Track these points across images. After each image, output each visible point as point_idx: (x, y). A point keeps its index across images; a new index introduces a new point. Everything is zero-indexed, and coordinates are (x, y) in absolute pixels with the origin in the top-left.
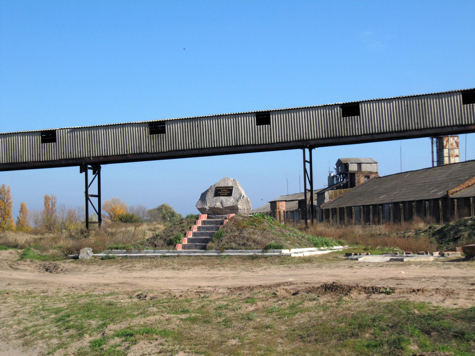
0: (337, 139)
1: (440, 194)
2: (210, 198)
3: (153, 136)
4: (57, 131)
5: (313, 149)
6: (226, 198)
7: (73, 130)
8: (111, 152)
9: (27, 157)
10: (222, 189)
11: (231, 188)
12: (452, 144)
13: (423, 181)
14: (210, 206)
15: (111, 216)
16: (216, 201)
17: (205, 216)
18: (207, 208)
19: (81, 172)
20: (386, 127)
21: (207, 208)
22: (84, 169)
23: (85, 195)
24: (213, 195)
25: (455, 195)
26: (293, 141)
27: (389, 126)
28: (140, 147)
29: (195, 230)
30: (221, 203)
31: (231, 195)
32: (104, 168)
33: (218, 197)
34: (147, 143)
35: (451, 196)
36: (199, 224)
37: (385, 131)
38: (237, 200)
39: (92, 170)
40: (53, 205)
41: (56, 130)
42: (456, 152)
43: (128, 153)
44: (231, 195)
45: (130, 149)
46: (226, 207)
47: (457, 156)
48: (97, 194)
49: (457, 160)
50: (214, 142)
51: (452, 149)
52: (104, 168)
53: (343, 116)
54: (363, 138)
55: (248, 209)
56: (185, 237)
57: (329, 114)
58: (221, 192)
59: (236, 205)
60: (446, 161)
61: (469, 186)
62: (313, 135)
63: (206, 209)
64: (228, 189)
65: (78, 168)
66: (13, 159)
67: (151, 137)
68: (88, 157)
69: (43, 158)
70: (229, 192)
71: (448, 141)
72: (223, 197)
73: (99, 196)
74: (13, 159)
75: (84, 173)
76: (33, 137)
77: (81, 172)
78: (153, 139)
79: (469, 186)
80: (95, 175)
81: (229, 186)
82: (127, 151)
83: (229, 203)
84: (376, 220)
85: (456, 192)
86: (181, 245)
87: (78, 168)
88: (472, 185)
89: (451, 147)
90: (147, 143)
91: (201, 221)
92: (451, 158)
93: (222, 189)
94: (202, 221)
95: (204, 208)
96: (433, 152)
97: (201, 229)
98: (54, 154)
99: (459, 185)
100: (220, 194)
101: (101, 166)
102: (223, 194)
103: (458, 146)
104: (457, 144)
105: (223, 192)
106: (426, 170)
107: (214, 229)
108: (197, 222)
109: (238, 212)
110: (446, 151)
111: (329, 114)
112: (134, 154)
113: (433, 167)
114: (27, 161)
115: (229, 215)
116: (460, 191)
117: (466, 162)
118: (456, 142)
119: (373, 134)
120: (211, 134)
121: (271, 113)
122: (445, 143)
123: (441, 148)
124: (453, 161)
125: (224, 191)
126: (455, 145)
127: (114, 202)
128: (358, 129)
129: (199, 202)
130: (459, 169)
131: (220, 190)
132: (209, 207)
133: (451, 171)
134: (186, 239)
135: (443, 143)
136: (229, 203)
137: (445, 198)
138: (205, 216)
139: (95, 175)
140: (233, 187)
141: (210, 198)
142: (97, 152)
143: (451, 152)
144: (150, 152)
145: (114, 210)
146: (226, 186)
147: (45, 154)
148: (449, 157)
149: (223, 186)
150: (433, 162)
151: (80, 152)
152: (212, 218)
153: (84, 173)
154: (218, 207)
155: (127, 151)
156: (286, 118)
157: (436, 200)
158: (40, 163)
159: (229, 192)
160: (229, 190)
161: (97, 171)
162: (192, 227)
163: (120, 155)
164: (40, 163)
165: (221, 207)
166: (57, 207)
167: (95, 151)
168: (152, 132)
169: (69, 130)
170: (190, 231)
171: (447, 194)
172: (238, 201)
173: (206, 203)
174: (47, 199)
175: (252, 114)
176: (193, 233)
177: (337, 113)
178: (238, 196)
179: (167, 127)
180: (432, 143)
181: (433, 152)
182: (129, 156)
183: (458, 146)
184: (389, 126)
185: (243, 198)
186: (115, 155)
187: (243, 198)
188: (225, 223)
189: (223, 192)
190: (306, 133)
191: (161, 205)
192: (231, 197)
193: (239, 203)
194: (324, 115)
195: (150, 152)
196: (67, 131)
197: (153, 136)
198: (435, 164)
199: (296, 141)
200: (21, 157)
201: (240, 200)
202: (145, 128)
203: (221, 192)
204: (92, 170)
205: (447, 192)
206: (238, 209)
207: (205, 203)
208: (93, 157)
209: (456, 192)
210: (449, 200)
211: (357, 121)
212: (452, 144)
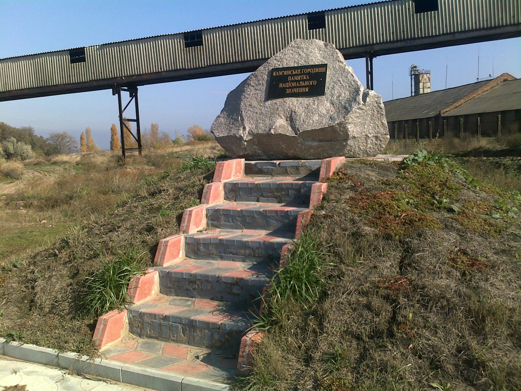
0: (409, 42)
1: (432, 114)
2: (255, 103)
3: (189, 49)
4: (85, 48)
5: (374, 58)
6: (305, 101)
7: (102, 46)
8: (144, 70)
9: (57, 80)
10: (292, 75)
11: (322, 70)
12: (425, 79)
13: (413, 105)
14: (255, 131)
15: (194, 136)
16: (273, 114)
17: (240, 163)
18: (246, 137)
19: (114, 94)
20: (472, 23)
21: (246, 137)
22: (116, 91)
23: (119, 120)
24: (262, 95)
25: (446, 115)
26: (353, 47)
27: (476, 22)
28: (175, 63)
29: (197, 225)
30: (291, 119)
31: (322, 93)
32: (142, 90)
33: (279, 101)
34: (183, 58)
35: (443, 115)
36: (216, 197)
37: (471, 29)
38: (345, 108)
39: (129, 92)
40: (157, 129)
41: (84, 47)
42: (428, 85)
43: (163, 70)
44: (322, 93)
45: (165, 66)
46: (306, 132)
47: (429, 88)
48: (136, 119)
49: (429, 91)
50: (259, 52)
51: (425, 83)
52: (142, 90)
53: (416, 13)
54: (442, 39)
55: (377, 138)
56: (153, 263)
57: (398, 10)
58: (288, 85)
59: (340, 124)
60: (421, 91)
61: (457, 107)
62: (377, 38)
63: (241, 138)
64: (309, 74)
65: (111, 90)
66: (43, 82)
67: (186, 50)
68: (120, 77)
69: (74, 80)
70: (315, 83)
71: (423, 77)
72: (294, 99)
73: (137, 120)
74: (43, 82)
75: (117, 95)
76: (62, 57)
77: (114, 94)
78: (189, 52)
79: (457, 107)
80: (131, 98)
81: (311, 63)
82: (161, 68)
83: (316, 118)
84: (402, 136)
85: (447, 112)
86: (125, 317)
87: (111, 90)
88: (459, 106)
89: (425, 81)
90: (183, 58)
91: (221, 188)
92: (425, 89)
93: (292, 75)
94: (207, 210)
95: (234, 136)
96: (411, 85)
97: (222, 218)
98: (84, 74)
99: (448, 106)
100: (284, 89)
101: (138, 87)
102: (296, 90)
103: (429, 81)
104: (429, 79)
105: (294, 84)
106: (487, 82)
107: (272, 221)
108: (208, 192)
109: (345, 146)
110: (421, 84)
111: (398, 10)
112: (169, 71)
113: (412, 96)
114: (57, 84)
115: (329, 164)
116: (449, 111)
117: (446, 89)
118: (428, 77)
119: (454, 33)
120: (255, 43)
121: (326, 13)
122: (421, 78)
123: (418, 82)
124: (426, 92)
125: (298, 81)
126: (427, 79)
127: (195, 127)
128: (435, 27)
129: (222, 120)
130: (442, 95)
131: (284, 79)
132: (251, 133)
133: (435, 96)
134: (182, 238)
135: (419, 79)
136: (316, 118)
137: (438, 117)
138: (239, 164)
139: (131, 98)
140: (325, 66)
141: (255, 103)
142: (128, 71)
143: (425, 85)
144: (187, 68)
145: (195, 132)
146: (302, 63)
147: (75, 76)
148: (423, 88)
149: (292, 65)
150: (412, 92)
151: (111, 72)
152: (260, 172)
153: (117, 95)
154: (280, 131)
155: (161, 68)
156: (344, 19)
157: (429, 119)
158: (70, 86)
159: (315, 83)
160: (312, 76)
161: (134, 94)
162: (186, 217)
163: (153, 73)
164: (70, 86)
165: (289, 132)
166: (160, 130)
167: (127, 70)
168: (187, 45)
169: (98, 47)
170: (177, 232)
171: (440, 114)
172: (346, 110)
173: (242, 120)
174: (152, 125)
175: (304, 16)
176: (187, 244)
177: (409, 9)
178: (346, 94)
179: (205, 38)
180: (411, 79)
181: (411, 85)
182: (164, 73)
183: (429, 81)
184: (476, 22)
185: (364, 100)
186: (148, 73)
187: (364, 100)
188: (315, 199)
189: (294, 84)
190: (369, 36)
191: (28, 126)
192: (323, 97)
193: (352, 117)
194: (391, 12)
195: (187, 68)
196: (96, 48)
197: (189, 49)
198: (413, 94)
199: (356, 46)
200: (51, 79)
201: (355, 107)
202: (180, 40)
203: (288, 85)
204: (129, 92)
205: (440, 112)
206: (346, 137)
207: (237, 120)
208: (125, 77)
209: (447, 112)
210: (441, 119)
211: (435, 17)
212: (425, 79)
